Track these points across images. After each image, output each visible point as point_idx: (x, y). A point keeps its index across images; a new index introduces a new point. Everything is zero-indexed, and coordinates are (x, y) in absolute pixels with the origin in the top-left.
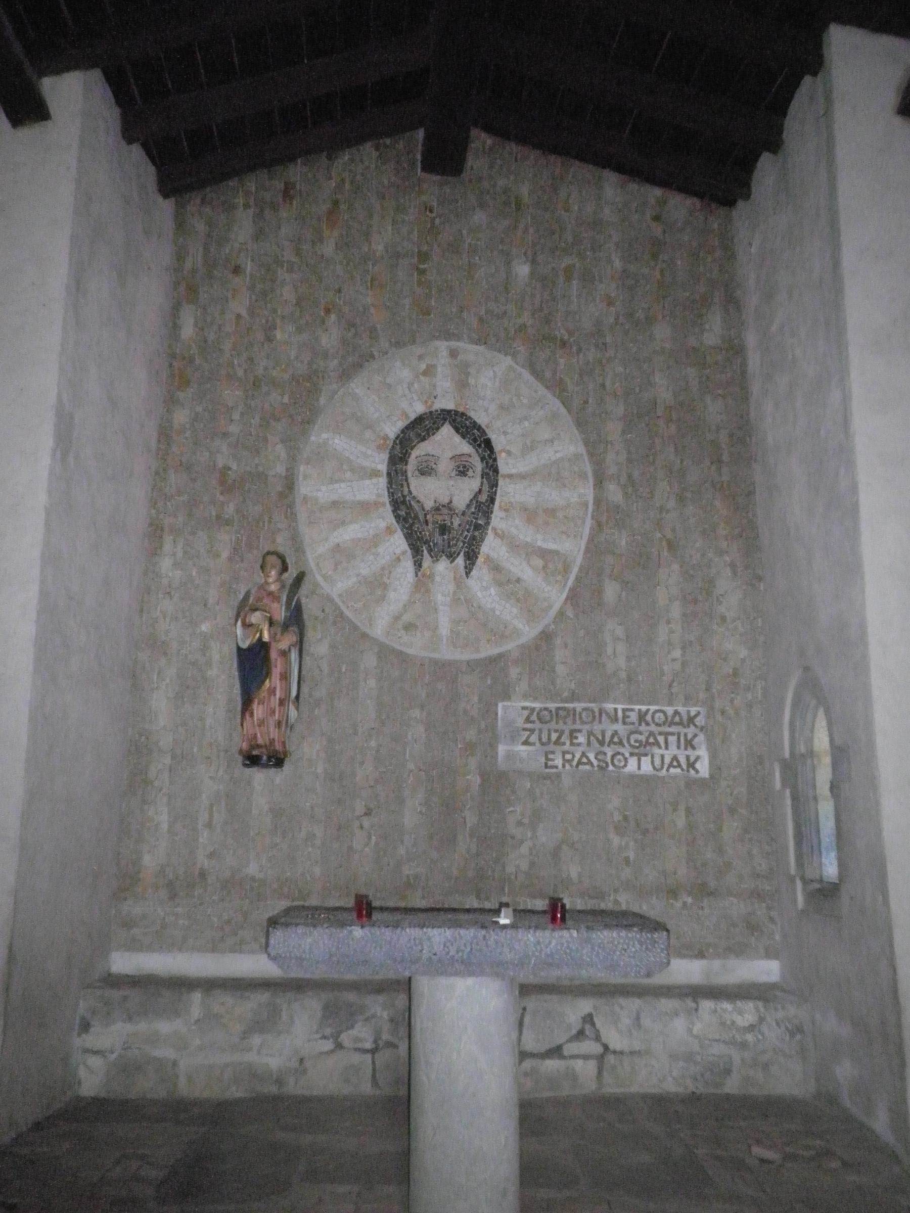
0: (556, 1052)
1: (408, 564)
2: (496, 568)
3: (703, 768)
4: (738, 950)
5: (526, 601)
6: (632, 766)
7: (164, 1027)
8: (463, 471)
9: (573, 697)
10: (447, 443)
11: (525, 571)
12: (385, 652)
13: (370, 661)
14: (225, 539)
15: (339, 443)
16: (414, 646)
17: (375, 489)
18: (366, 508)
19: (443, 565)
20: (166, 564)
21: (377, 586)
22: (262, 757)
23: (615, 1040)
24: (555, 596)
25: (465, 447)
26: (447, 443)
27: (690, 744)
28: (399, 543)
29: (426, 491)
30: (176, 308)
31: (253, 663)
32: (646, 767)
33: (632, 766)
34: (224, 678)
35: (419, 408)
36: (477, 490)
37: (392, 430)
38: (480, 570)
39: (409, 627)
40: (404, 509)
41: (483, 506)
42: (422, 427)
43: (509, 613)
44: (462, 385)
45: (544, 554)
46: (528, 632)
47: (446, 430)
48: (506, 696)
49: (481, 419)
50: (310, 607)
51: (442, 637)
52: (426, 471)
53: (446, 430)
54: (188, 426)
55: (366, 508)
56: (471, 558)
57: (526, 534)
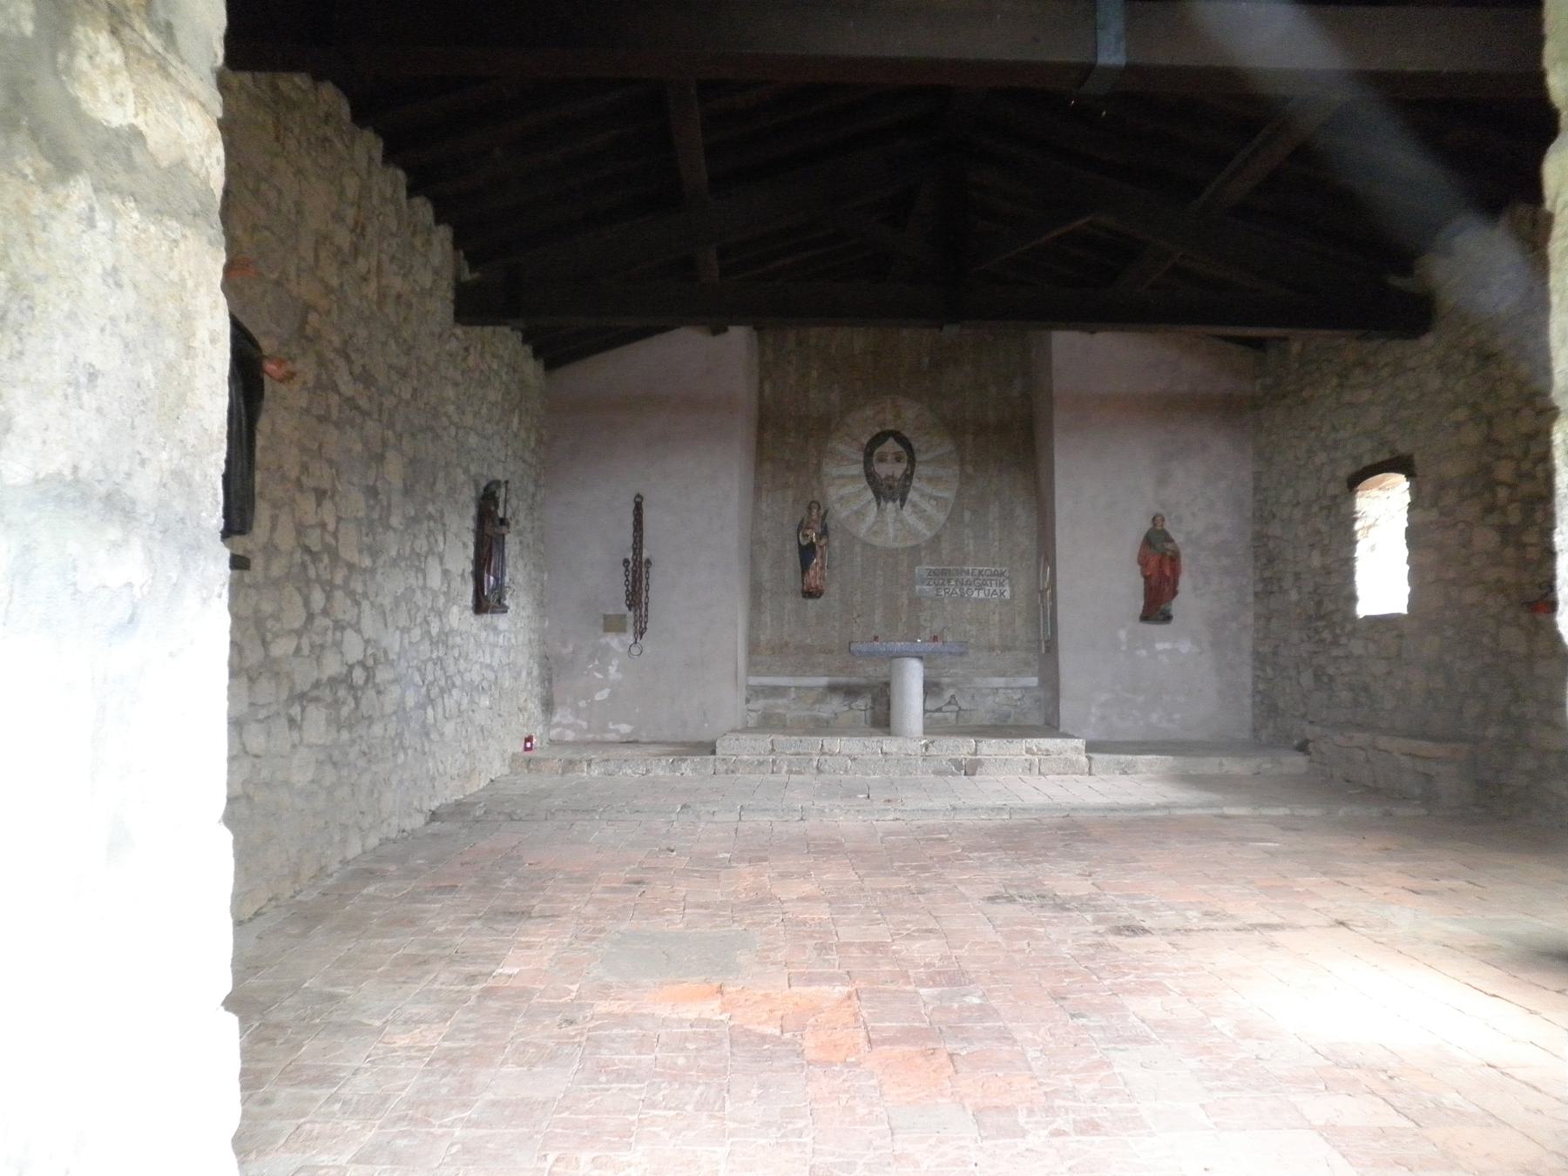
0: (939, 710)
1: (874, 504)
2: (914, 505)
3: (1007, 595)
4: (1019, 673)
5: (928, 520)
6: (975, 594)
7: (780, 701)
8: (898, 460)
9: (950, 563)
10: (891, 446)
11: (929, 507)
12: (865, 545)
13: (858, 549)
14: (790, 493)
15: (841, 447)
16: (878, 541)
17: (858, 469)
18: (853, 478)
19: (890, 505)
20: (764, 507)
21: (860, 514)
22: (810, 593)
23: (964, 705)
24: (941, 517)
25: (899, 448)
26: (891, 446)
27: (1001, 584)
28: (870, 495)
29: (883, 470)
30: (761, 381)
31: (807, 553)
32: (982, 595)
33: (975, 594)
34: (793, 558)
35: (878, 430)
36: (733, 736)
37: (865, 440)
38: (907, 507)
39: (875, 533)
40: (870, 476)
41: (908, 477)
42: (879, 439)
43: (921, 526)
44: (898, 416)
45: (936, 498)
46: (929, 534)
47: (891, 441)
48: (920, 563)
49: (907, 434)
50: (831, 524)
51: (890, 536)
52: (882, 460)
53: (891, 441)
54: (305, 458)
55: (853, 478)
56: (903, 500)
57: (928, 489)
